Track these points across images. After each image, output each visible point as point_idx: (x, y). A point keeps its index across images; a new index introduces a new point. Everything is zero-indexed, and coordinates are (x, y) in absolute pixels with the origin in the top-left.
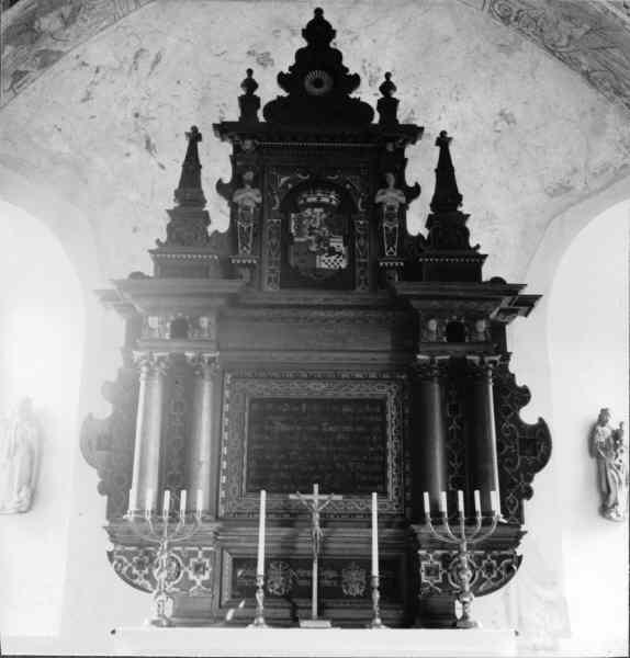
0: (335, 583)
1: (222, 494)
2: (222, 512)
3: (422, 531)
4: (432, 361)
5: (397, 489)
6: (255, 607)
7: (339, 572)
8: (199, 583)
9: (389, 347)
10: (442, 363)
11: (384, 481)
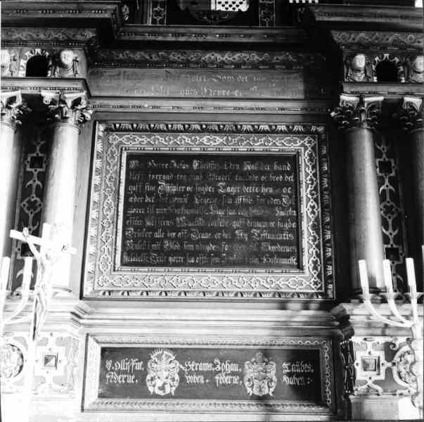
0: (236, 380)
3: (356, 312)
4: (361, 103)
5: (315, 263)
7: (241, 366)
9: (301, 96)
10: (373, 106)
11: (298, 254)
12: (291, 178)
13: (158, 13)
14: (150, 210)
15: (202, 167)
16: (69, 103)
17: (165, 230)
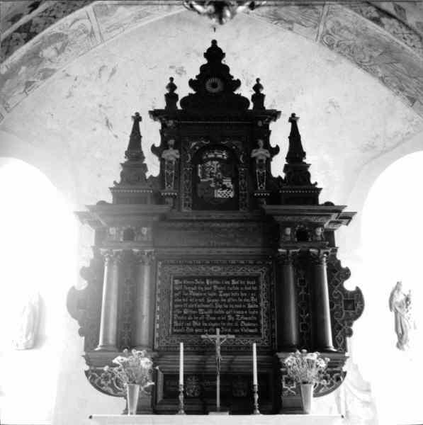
4: (288, 252)
12: (255, 288)
13: (187, 200)
14: (186, 305)
15: (211, 283)
16: (146, 254)
17: (193, 316)
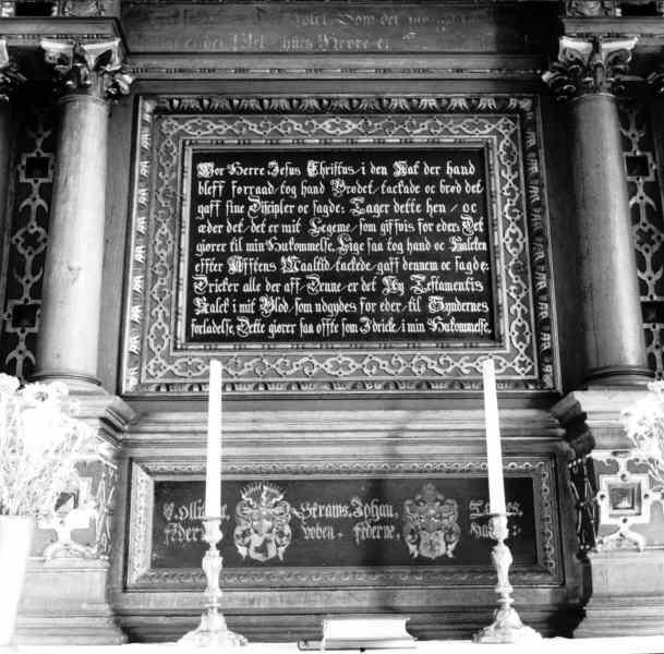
1: (131, 343)
2: (129, 384)
6: (204, 587)
8: (64, 535)
9: (491, 48)
10: (617, 57)
